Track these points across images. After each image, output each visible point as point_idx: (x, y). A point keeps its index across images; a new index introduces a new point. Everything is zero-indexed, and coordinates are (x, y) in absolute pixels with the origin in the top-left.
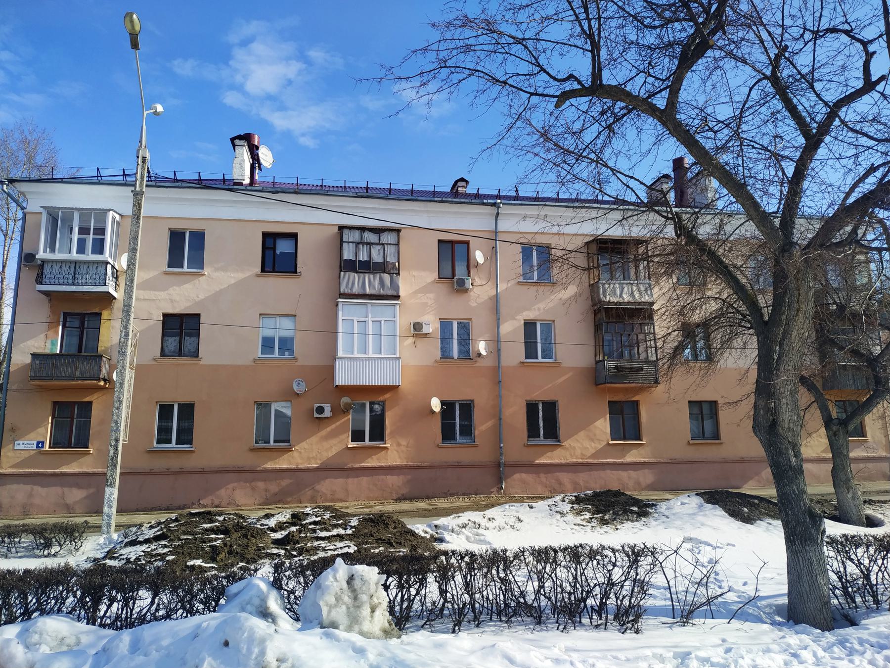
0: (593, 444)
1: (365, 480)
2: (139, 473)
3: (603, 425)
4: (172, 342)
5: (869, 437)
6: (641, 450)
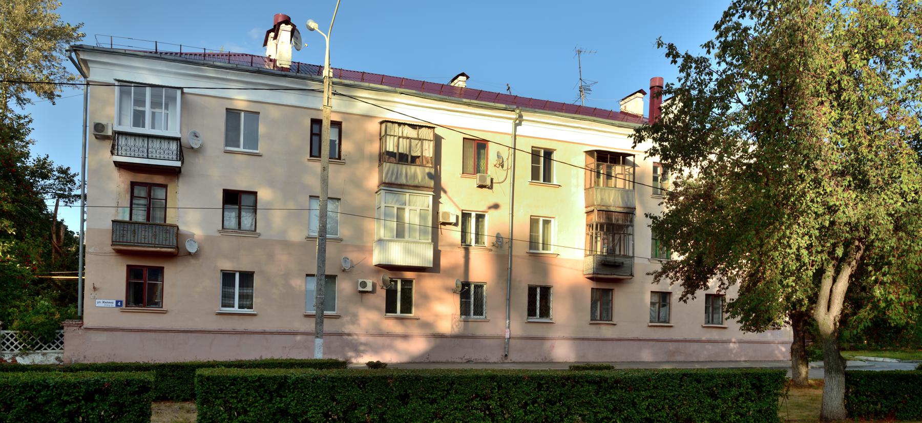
2: (209, 332)
4: (231, 216)
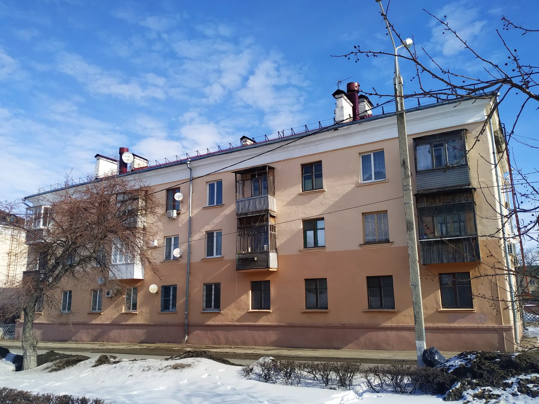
0: (239, 312)
1: (127, 331)
3: (248, 298)
5: (475, 309)
6: (269, 316)
